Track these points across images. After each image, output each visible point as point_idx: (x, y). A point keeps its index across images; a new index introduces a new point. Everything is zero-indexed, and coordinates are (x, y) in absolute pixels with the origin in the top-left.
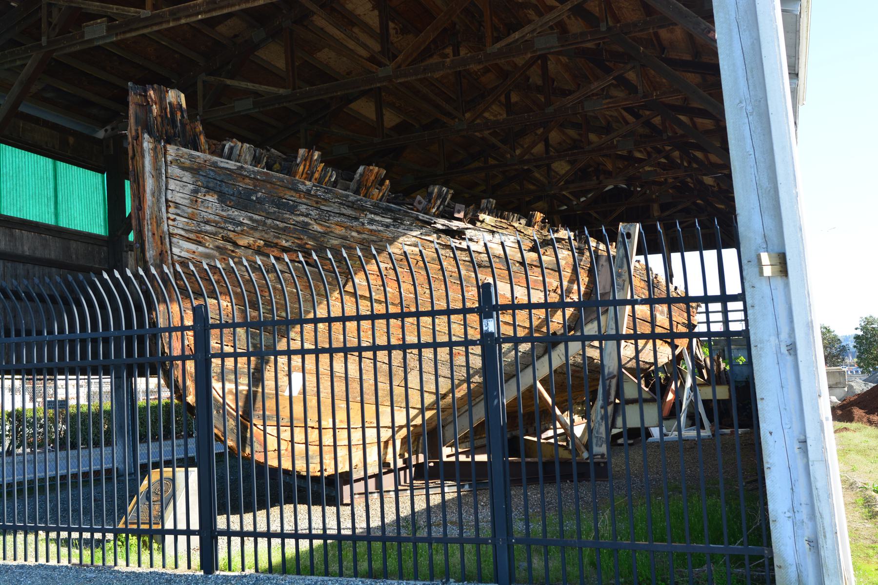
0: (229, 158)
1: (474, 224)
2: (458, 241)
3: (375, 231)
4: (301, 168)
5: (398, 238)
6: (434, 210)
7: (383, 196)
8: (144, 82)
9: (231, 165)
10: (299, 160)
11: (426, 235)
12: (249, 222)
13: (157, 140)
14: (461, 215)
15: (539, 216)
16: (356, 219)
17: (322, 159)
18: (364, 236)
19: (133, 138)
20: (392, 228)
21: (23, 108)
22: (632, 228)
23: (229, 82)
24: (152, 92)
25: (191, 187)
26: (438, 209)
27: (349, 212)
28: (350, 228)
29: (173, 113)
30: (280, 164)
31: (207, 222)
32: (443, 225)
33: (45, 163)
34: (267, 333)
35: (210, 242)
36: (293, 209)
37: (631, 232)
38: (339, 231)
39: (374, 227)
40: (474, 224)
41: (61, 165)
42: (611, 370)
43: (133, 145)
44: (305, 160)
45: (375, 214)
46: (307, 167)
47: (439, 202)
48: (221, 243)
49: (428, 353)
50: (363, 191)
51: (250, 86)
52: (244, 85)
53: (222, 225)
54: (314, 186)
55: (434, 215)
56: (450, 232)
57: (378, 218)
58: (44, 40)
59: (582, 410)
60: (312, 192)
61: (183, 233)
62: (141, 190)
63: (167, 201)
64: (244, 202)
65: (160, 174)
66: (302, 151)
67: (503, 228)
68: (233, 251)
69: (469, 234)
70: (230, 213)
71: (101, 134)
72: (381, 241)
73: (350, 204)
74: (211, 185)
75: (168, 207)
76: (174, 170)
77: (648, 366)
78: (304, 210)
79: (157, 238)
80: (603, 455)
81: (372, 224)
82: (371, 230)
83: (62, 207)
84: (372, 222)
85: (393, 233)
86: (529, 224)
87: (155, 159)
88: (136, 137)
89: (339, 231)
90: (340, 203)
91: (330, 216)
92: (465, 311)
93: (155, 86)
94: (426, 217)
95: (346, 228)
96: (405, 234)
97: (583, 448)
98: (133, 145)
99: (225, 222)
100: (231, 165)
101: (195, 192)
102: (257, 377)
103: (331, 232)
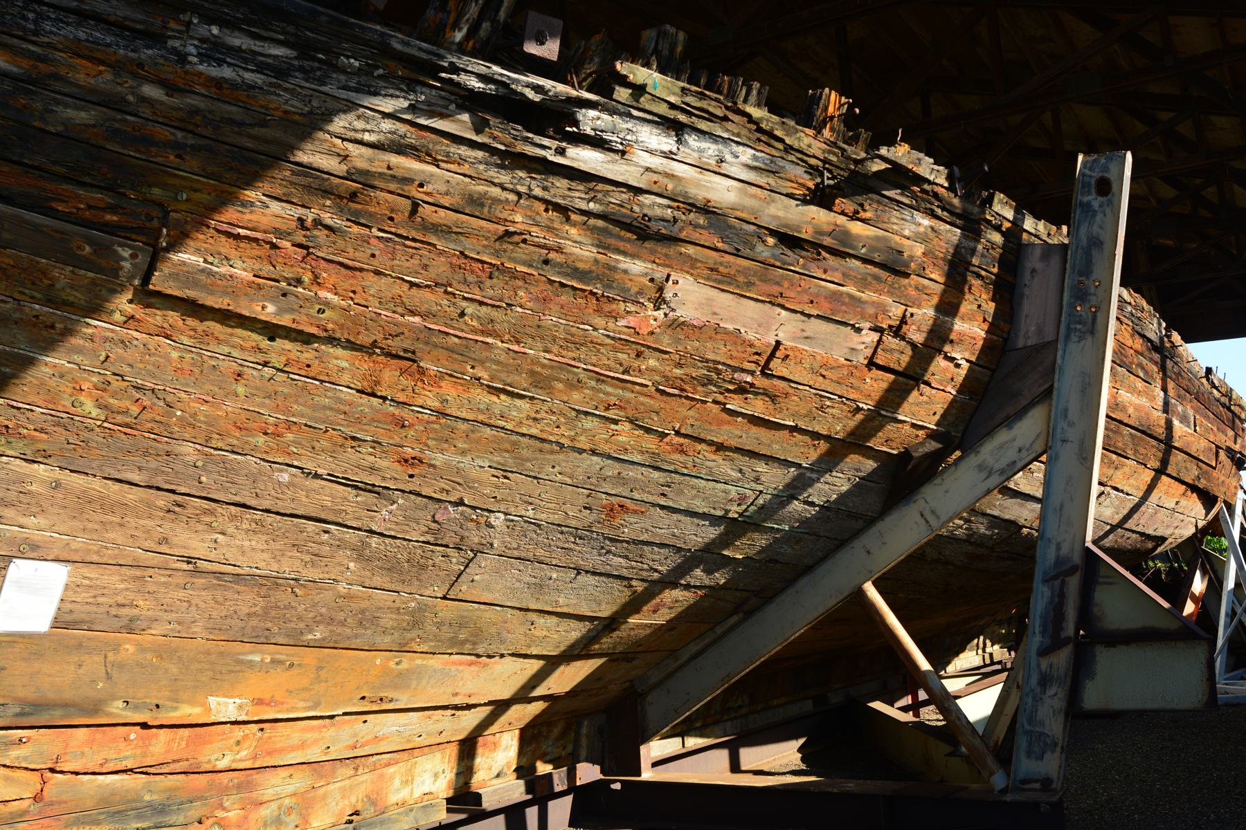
2: (554, 144)
3: (234, 86)
5: (328, 117)
11: (431, 114)
14: (550, 50)
15: (834, 102)
16: (155, 38)
18: (191, 100)
20: (298, 80)
22: (1113, 167)
28: (137, 70)
32: (482, 78)
37: (1112, 176)
39: (227, 72)
40: (608, 93)
42: (1065, 550)
55: (461, 50)
56: (509, 107)
59: (1009, 633)
67: (712, 117)
69: (590, 120)
72: (264, 124)
77: (1150, 545)
80: (1046, 783)
81: (220, 62)
82: (219, 83)
84: (215, 52)
85: (307, 100)
86: (807, 116)
91: (40, 17)
94: (418, 48)
95: (117, 67)
96: (351, 106)
97: (991, 761)
103: (56, 77)
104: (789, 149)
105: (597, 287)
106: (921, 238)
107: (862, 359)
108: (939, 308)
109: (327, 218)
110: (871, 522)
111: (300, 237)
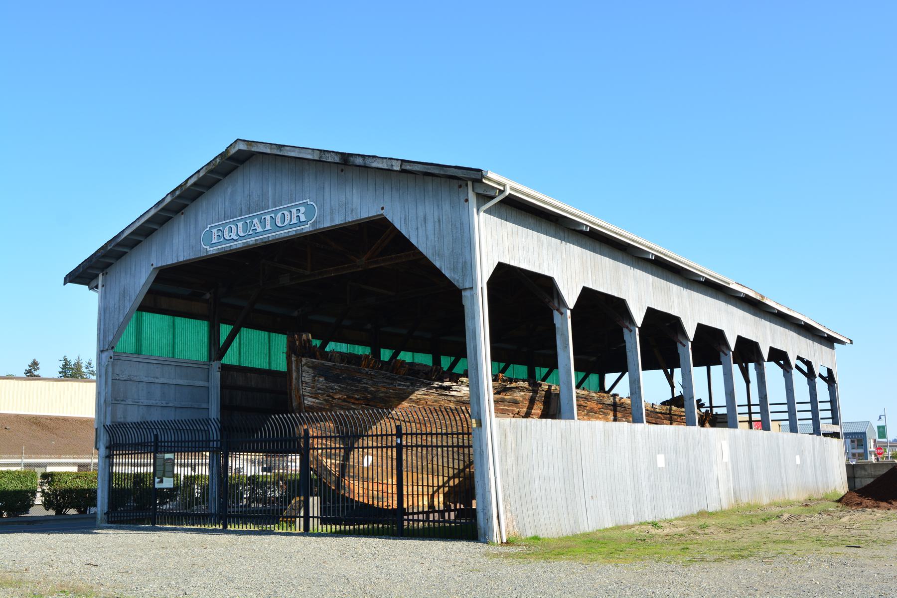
9: (330, 364)
13: (297, 356)
31: (320, 389)
33: (264, 335)
34: (349, 439)
36: (360, 381)
38: (383, 390)
41: (273, 335)
49: (414, 449)
64: (336, 379)
69: (454, 388)
71: (296, 314)
76: (305, 368)
83: (273, 358)
84: (400, 385)
89: (383, 390)
92: (392, 435)
101: (314, 377)
102: (346, 458)
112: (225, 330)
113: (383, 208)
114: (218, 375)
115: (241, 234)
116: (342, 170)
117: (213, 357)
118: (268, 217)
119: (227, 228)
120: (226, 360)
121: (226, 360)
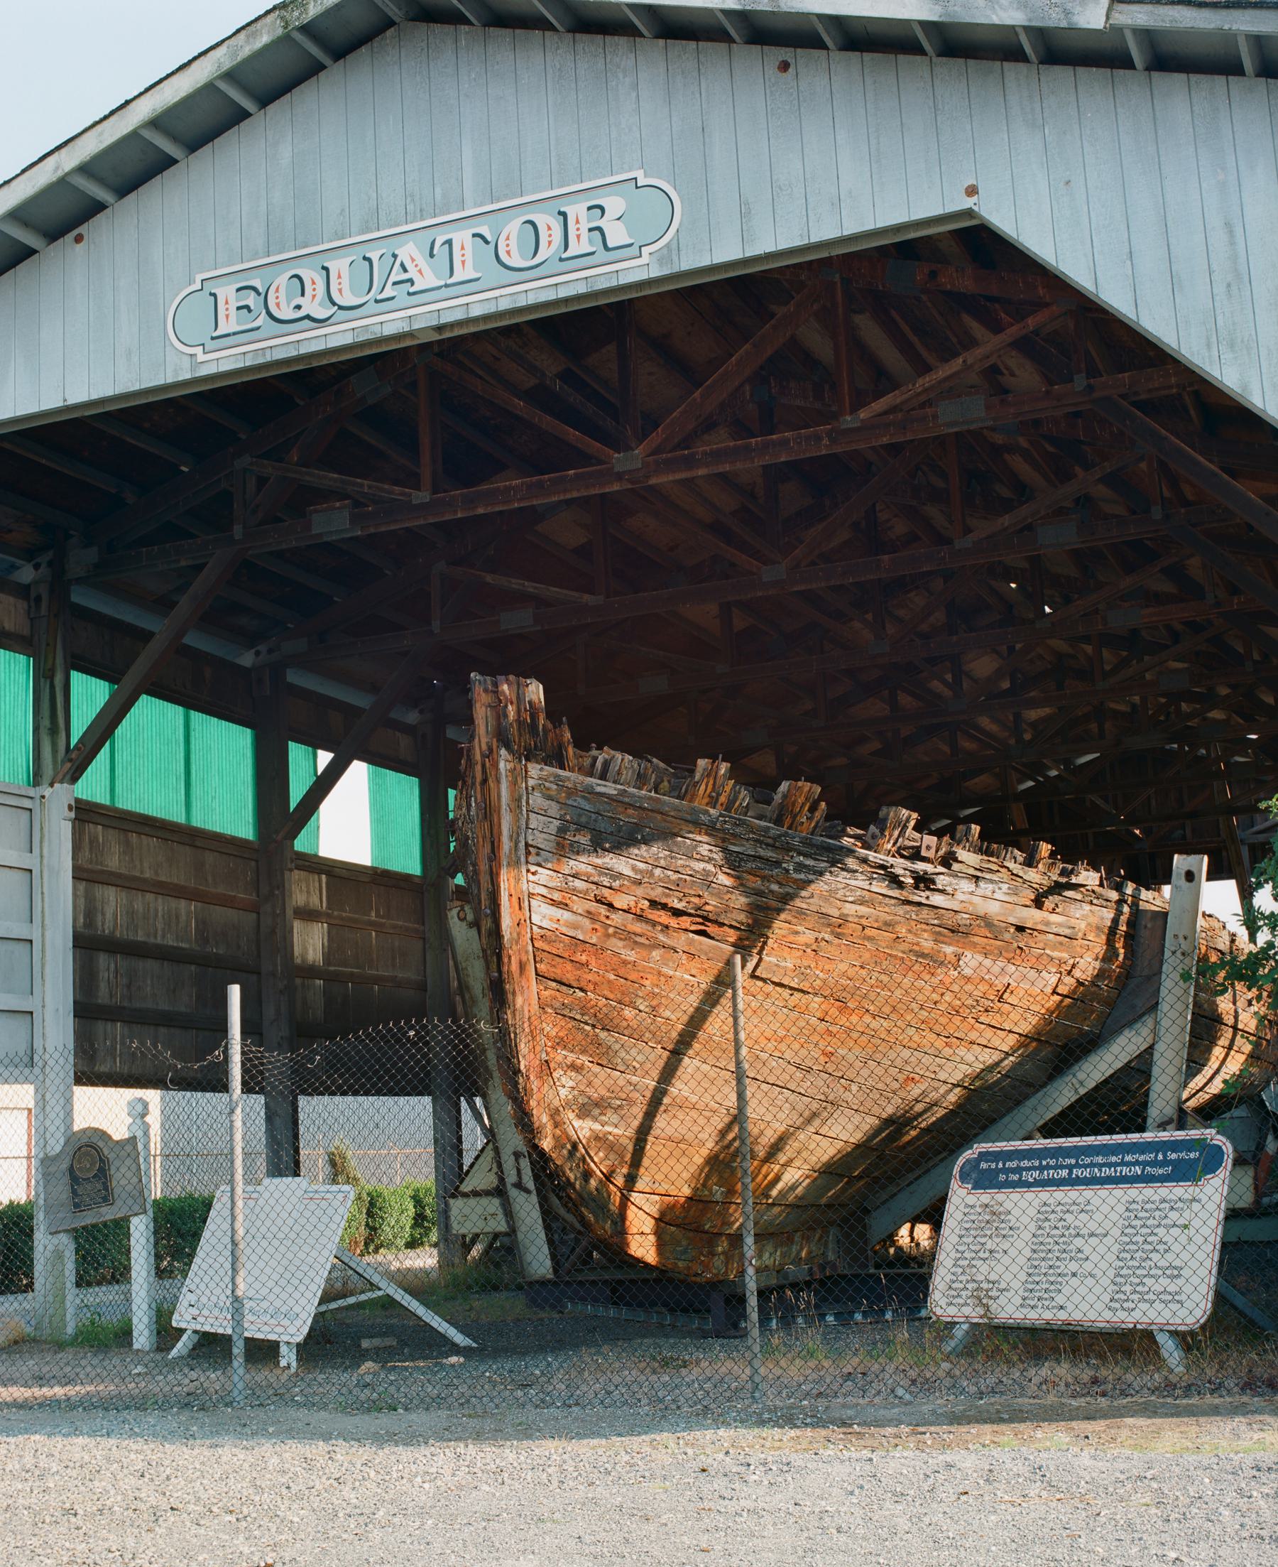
0: (603, 777)
1: (949, 867)
4: (703, 787)
6: (889, 846)
7: (815, 827)
8: (494, 670)
9: (609, 788)
10: (697, 777)
12: (631, 874)
13: (517, 755)
16: (778, 864)
17: (732, 774)
19: (483, 756)
21: (188, 640)
23: (489, 578)
24: (505, 687)
25: (557, 823)
26: (894, 844)
27: (769, 854)
29: (534, 716)
30: (669, 782)
35: (579, 905)
39: (802, 876)
40: (949, 867)
41: (196, 716)
43: (483, 766)
44: (708, 776)
45: (805, 855)
46: (710, 786)
47: (896, 833)
48: (593, 906)
50: (787, 822)
51: (530, 587)
52: (516, 584)
53: (595, 879)
54: (721, 815)
57: (810, 862)
58: (238, 531)
60: (718, 826)
61: (544, 891)
62: (495, 831)
63: (527, 845)
65: (520, 807)
66: (702, 763)
67: (991, 871)
68: (607, 917)
69: (941, 881)
70: (607, 860)
71: (247, 659)
73: (770, 841)
74: (583, 820)
75: (528, 853)
76: (537, 800)
78: (705, 853)
79: (515, 900)
86: (1030, 862)
87: (514, 783)
88: (490, 754)
90: (757, 841)
93: (511, 677)
95: (763, 878)
98: (483, 766)
99: (601, 874)
100: (609, 788)
101: (562, 830)
104: (1025, 881)
105: (933, 961)
106: (1084, 918)
107: (1049, 990)
108: (631, 1166)
109: (827, 937)
110: (1044, 1085)
111: (814, 947)
112: (88, 696)
113: (972, 191)
114: (67, 828)
115: (347, 299)
116: (784, 66)
117: (48, 770)
118: (462, 237)
119: (282, 280)
120: (92, 786)
121: (92, 786)
